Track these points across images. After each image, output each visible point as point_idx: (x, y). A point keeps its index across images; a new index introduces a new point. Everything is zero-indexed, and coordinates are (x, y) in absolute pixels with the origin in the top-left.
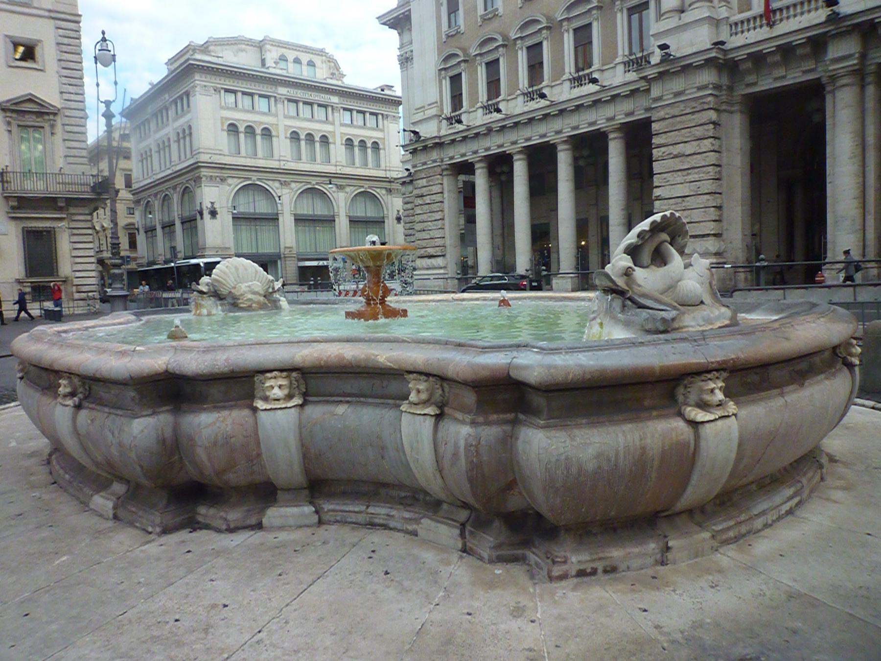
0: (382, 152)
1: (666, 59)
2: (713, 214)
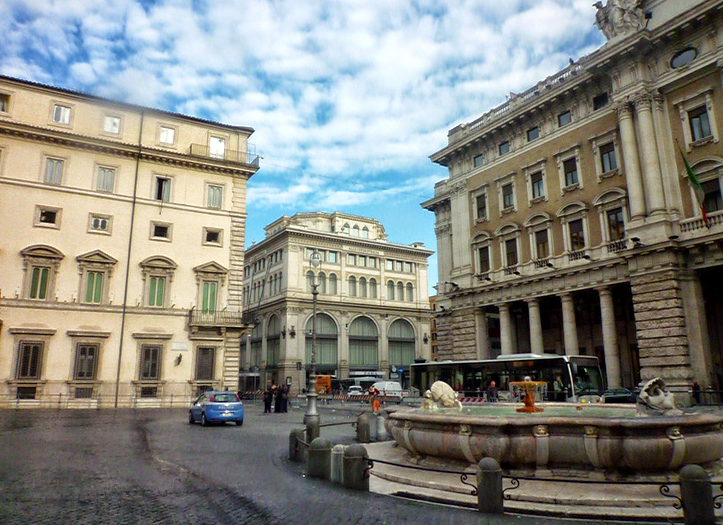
0: (414, 290)
1: (638, 246)
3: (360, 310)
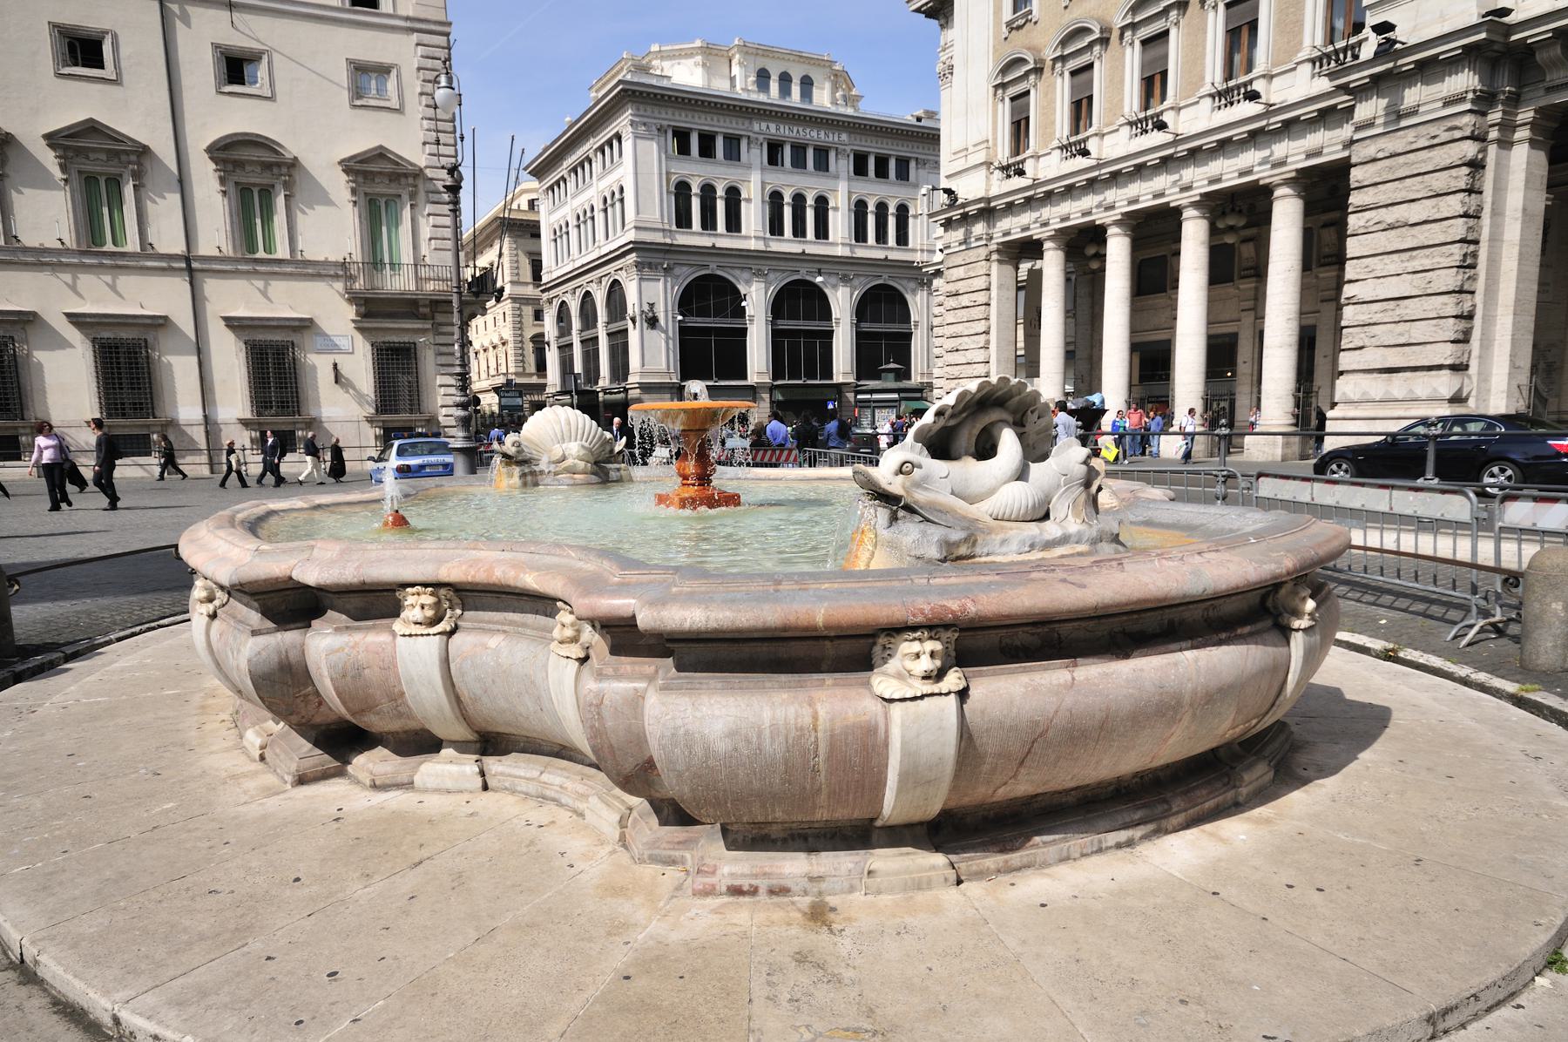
1: (1387, 50)
2: (1451, 329)
3: (878, 271)
